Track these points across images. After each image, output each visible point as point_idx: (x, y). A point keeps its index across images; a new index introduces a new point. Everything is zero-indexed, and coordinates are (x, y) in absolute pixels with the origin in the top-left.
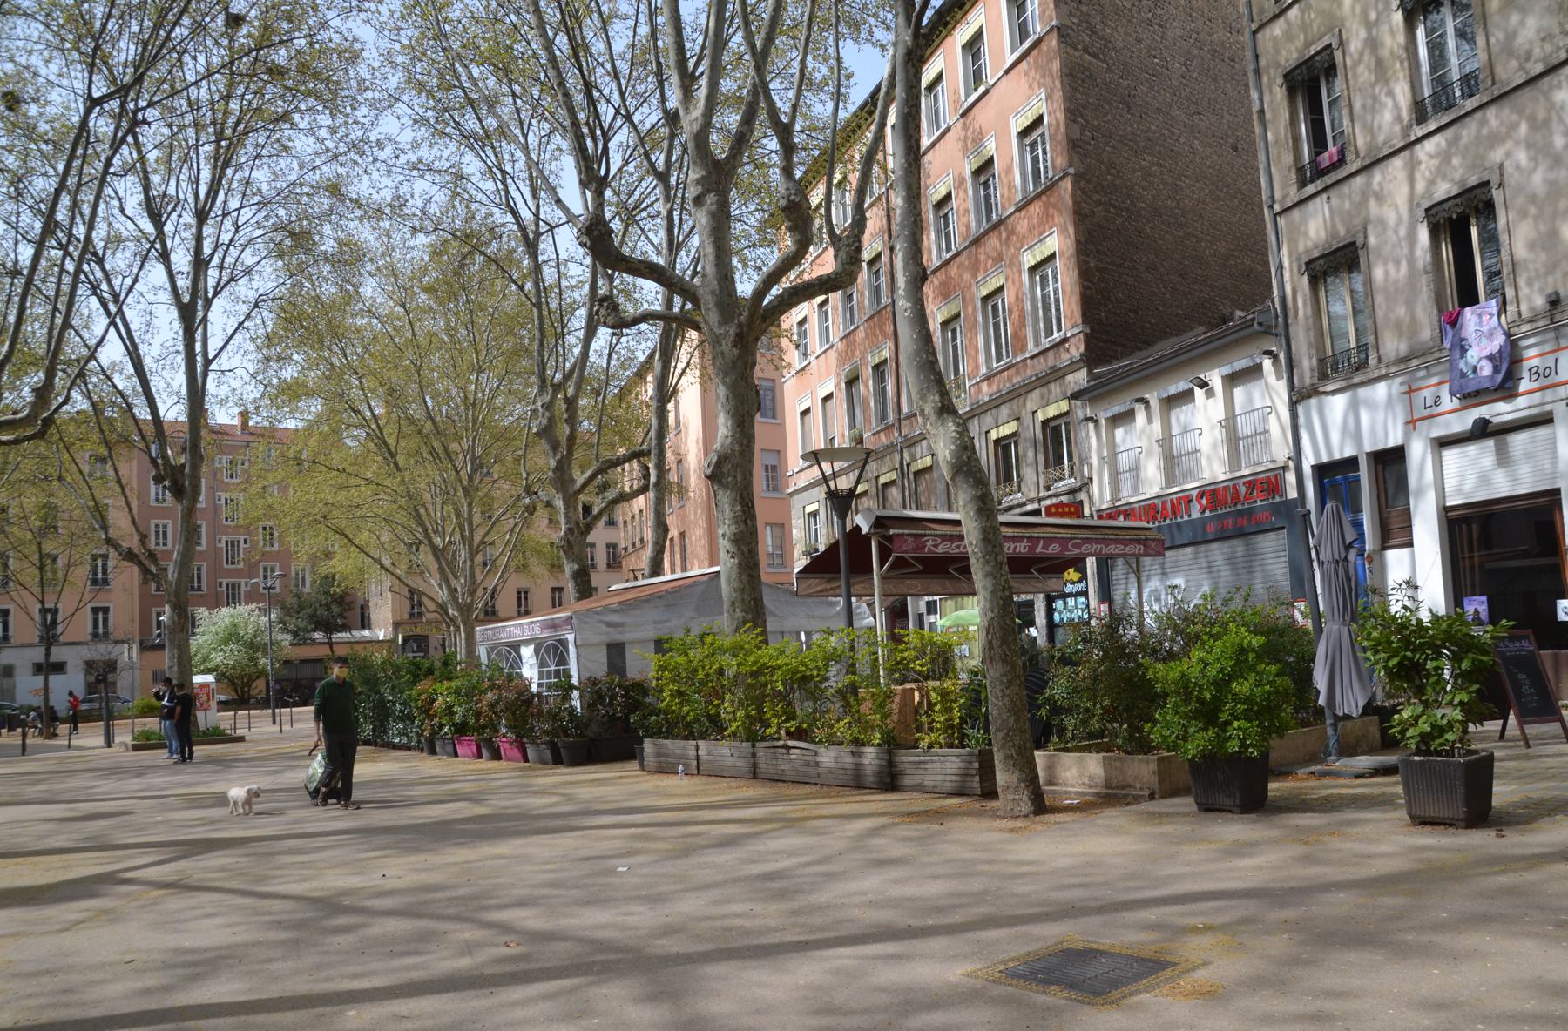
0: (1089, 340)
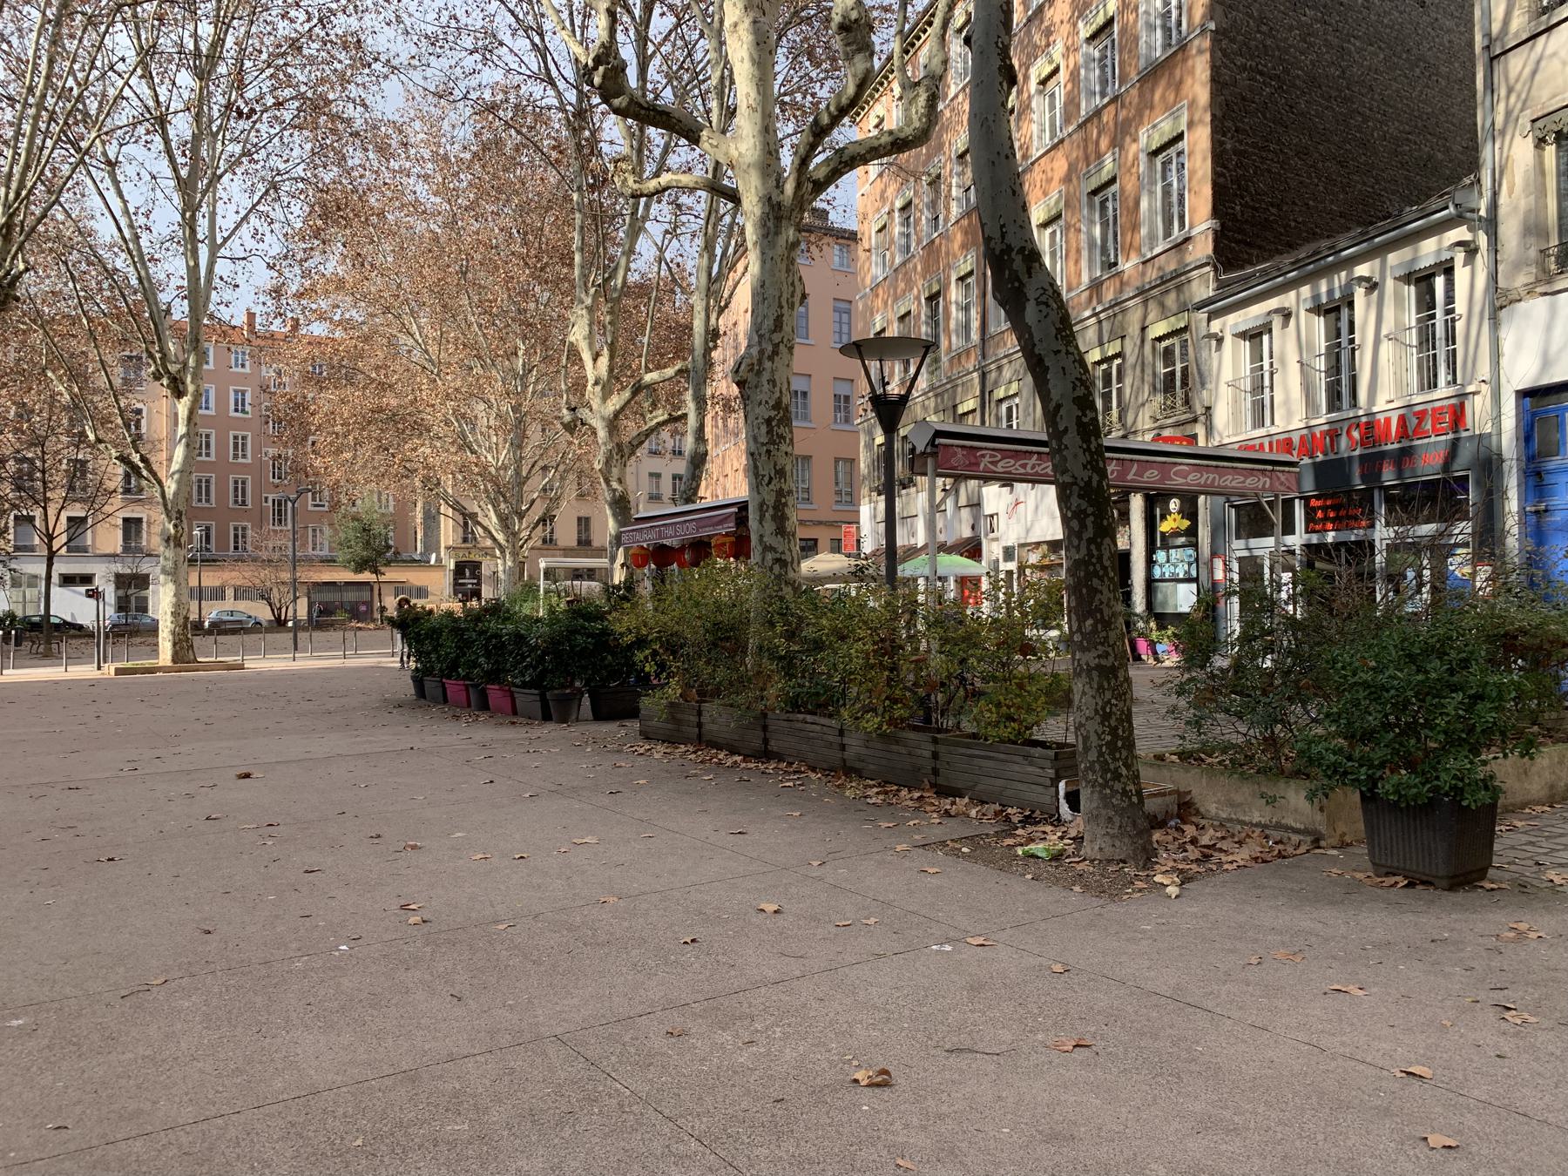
0: (1219, 238)
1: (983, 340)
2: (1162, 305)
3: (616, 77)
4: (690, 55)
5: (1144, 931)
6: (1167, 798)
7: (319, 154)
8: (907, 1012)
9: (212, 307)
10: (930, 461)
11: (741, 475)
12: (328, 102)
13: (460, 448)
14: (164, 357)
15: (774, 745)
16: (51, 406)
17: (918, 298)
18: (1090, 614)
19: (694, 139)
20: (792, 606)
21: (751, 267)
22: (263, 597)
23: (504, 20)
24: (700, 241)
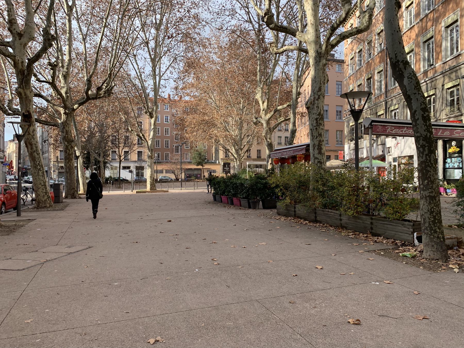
1: (386, 92)
2: (450, 77)
3: (271, 19)
4: (292, 10)
5: (447, 283)
6: (453, 240)
7: (187, 50)
8: (365, 302)
9: (160, 93)
10: (370, 130)
11: (306, 136)
12: (190, 34)
13: (225, 131)
14: (148, 108)
15: (318, 218)
16: (120, 121)
17: (364, 79)
18: (427, 179)
19: (295, 36)
20: (323, 176)
21: (310, 74)
22: (173, 173)
23: (238, 6)
24: (295, 66)
